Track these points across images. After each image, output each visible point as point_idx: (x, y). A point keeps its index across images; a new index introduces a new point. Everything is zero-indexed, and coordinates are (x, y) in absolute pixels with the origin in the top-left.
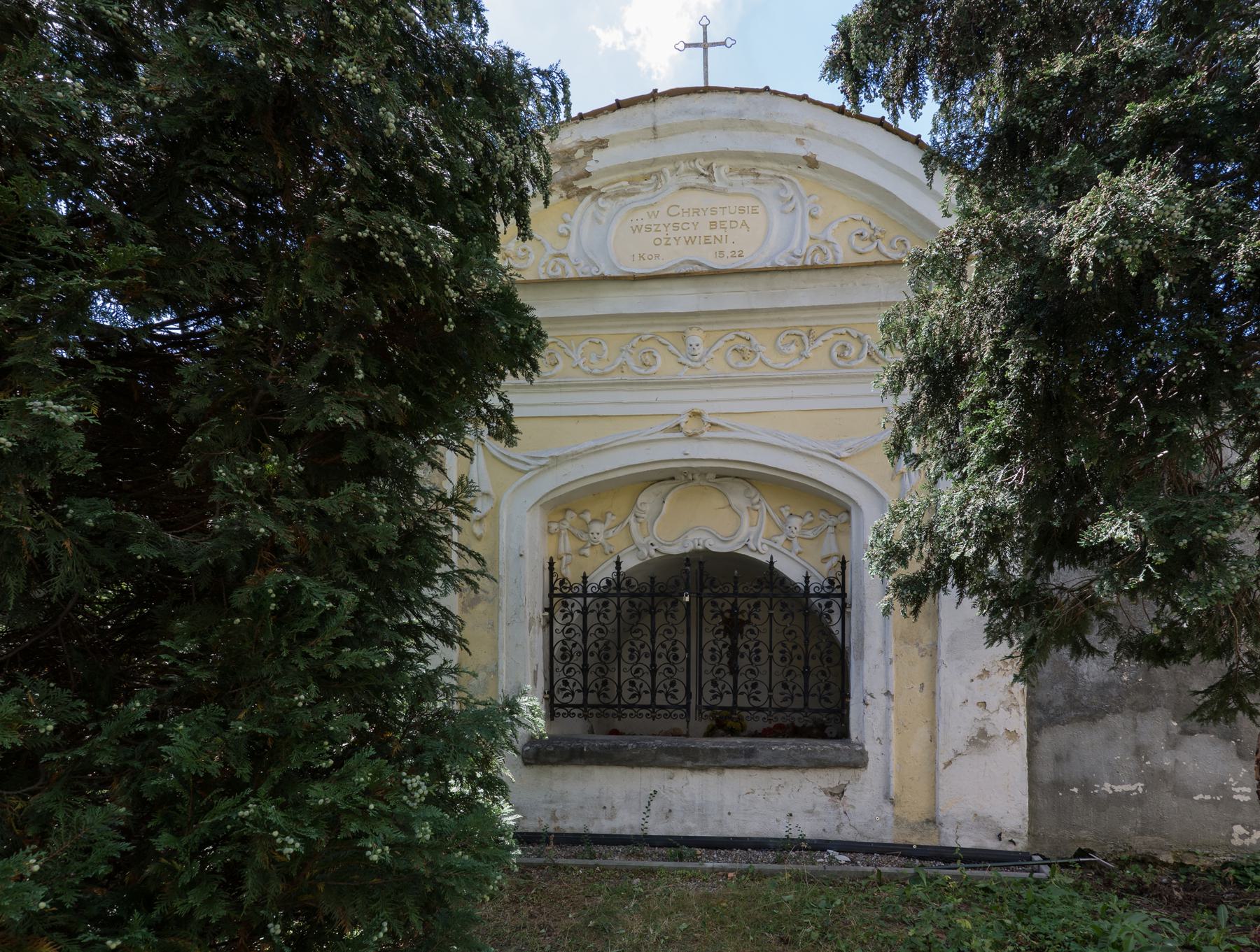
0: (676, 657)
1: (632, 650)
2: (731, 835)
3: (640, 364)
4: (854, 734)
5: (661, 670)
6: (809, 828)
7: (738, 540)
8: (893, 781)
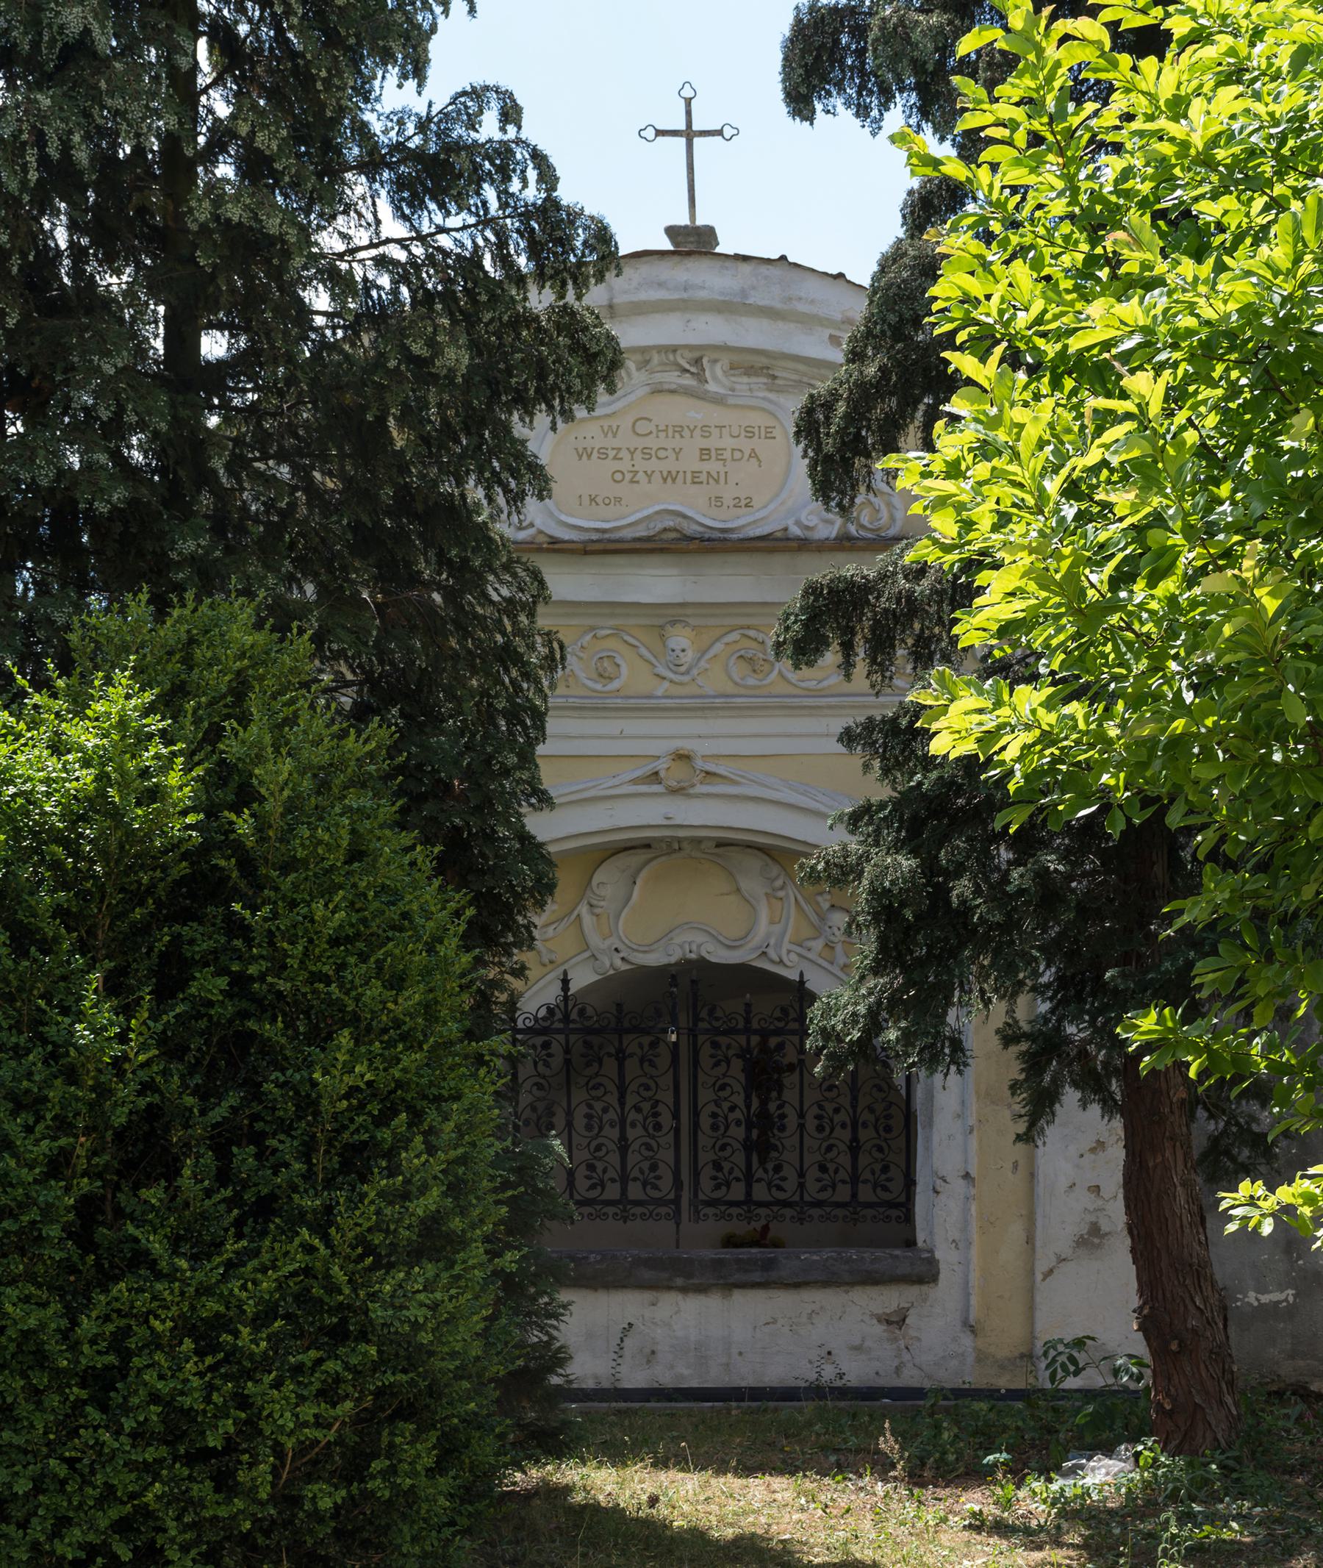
0: (658, 1127)
1: (589, 1117)
2: (743, 1384)
3: (595, 676)
4: (921, 1237)
5: (635, 1146)
6: (856, 1372)
7: (751, 945)
8: (974, 1300)
